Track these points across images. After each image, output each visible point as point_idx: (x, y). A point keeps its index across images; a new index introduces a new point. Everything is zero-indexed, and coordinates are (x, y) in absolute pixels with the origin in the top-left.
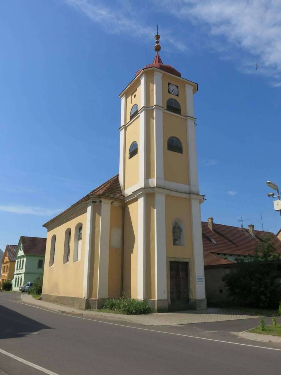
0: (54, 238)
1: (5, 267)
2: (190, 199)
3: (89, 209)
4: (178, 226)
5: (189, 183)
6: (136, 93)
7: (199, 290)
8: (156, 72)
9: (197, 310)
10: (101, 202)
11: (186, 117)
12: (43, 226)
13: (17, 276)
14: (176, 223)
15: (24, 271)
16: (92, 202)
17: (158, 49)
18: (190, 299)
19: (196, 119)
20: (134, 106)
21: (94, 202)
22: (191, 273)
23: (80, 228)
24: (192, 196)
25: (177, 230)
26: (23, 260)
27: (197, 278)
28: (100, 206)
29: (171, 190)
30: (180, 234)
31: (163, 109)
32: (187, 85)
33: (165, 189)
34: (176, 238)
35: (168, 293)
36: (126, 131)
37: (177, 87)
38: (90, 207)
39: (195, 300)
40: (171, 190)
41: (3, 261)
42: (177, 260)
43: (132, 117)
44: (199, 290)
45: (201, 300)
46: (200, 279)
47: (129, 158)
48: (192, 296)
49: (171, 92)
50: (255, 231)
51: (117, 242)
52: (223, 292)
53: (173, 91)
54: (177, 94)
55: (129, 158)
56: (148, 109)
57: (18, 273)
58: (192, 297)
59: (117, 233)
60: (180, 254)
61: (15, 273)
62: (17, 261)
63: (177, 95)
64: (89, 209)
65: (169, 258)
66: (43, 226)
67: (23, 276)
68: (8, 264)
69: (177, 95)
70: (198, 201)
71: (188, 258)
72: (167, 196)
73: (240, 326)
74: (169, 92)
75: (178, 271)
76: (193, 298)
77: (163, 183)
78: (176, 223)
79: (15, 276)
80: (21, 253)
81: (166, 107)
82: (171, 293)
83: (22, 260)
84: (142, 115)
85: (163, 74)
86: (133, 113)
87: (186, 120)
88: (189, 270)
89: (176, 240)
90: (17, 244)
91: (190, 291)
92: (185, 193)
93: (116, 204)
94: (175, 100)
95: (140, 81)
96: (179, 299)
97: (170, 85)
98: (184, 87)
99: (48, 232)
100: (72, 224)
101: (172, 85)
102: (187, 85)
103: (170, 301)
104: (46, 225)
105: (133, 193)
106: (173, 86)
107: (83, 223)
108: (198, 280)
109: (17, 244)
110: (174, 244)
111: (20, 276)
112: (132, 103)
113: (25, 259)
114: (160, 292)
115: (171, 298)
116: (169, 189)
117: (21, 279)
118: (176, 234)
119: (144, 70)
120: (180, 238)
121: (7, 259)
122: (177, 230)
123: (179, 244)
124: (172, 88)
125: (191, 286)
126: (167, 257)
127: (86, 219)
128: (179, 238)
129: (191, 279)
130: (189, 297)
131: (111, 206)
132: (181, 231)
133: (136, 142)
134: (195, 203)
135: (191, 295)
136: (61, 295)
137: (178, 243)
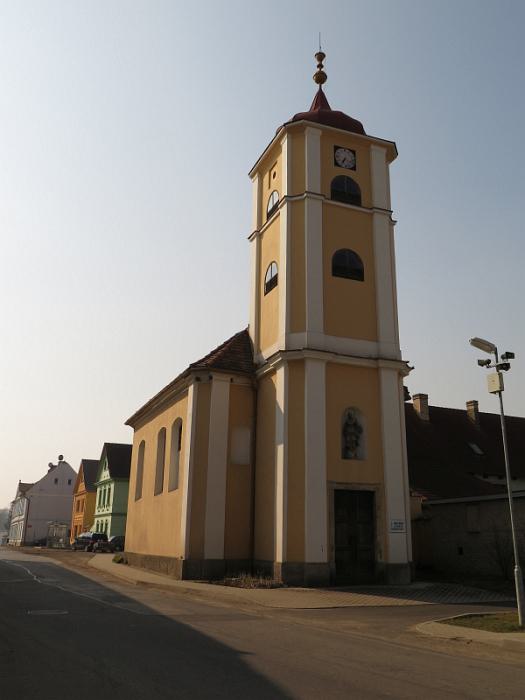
0: (143, 444)
1: (79, 501)
2: (377, 369)
3: (191, 389)
6: (275, 169)
7: (396, 545)
8: (308, 128)
10: (211, 378)
12: (127, 424)
13: (100, 519)
14: (350, 417)
15: (111, 511)
17: (321, 78)
21: (198, 379)
23: (178, 426)
24: (382, 364)
26: (109, 489)
28: (210, 385)
29: (336, 354)
30: (357, 437)
31: (323, 198)
32: (372, 147)
33: (328, 352)
36: (263, 241)
37: (354, 152)
38: (192, 387)
39: (388, 566)
40: (336, 354)
41: (76, 490)
42: (350, 488)
44: (396, 545)
45: (398, 567)
46: (398, 526)
47: (265, 294)
49: (340, 162)
55: (265, 294)
56: (293, 199)
57: (101, 513)
58: (380, 560)
59: (243, 438)
60: (355, 475)
61: (97, 513)
62: (98, 490)
63: (354, 168)
64: (191, 389)
66: (127, 424)
67: (109, 518)
68: (84, 497)
69: (354, 168)
70: (396, 373)
71: (372, 482)
72: (329, 364)
73: (422, 615)
74: (336, 164)
75: (354, 508)
76: (383, 560)
77: (321, 340)
78: (350, 417)
79: (96, 520)
80: (105, 475)
81: (328, 194)
82: (338, 550)
83: (107, 487)
84: (283, 211)
85: (323, 130)
87: (372, 214)
90: (99, 458)
92: (370, 358)
93: (240, 381)
94: (348, 178)
95: (281, 147)
96: (353, 565)
97: (339, 151)
100: (165, 419)
102: (372, 147)
103: (333, 566)
104: (129, 423)
109: (99, 458)
110: (345, 456)
111: (104, 519)
113: (112, 486)
114: (318, 549)
116: (331, 350)
117: (106, 525)
118: (351, 435)
120: (357, 444)
121: (82, 487)
122: (351, 430)
123: (356, 457)
124: (342, 155)
127: (186, 408)
135: (379, 556)
136: (152, 552)
137: (352, 454)
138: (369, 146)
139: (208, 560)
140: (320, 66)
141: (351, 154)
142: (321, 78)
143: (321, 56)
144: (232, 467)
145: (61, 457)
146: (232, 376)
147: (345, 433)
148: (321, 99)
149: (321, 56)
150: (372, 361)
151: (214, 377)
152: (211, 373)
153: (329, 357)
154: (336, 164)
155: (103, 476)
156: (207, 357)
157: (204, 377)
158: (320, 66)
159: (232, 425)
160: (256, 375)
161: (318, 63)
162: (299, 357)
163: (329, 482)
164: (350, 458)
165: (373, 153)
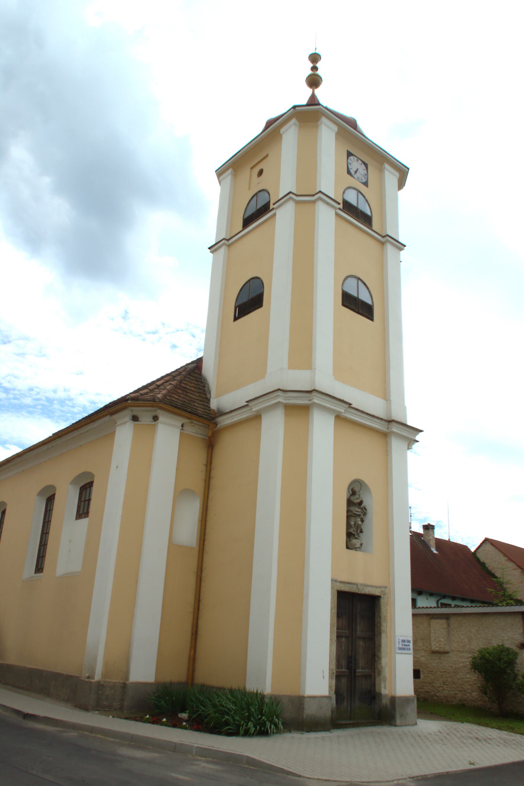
4: (358, 501)
5: (385, 395)
9: (395, 726)
10: (155, 418)
11: (383, 237)
14: (353, 493)
16: (131, 418)
18: (380, 694)
19: (405, 246)
20: (256, 194)
21: (135, 418)
22: (385, 626)
25: (356, 510)
27: (397, 640)
30: (362, 521)
32: (387, 166)
34: (351, 530)
35: (331, 677)
37: (366, 165)
39: (393, 699)
42: (354, 589)
43: (247, 222)
45: (406, 700)
48: (385, 688)
49: (352, 172)
50: (436, 539)
51: (188, 534)
52: (422, 676)
53: (358, 172)
54: (364, 181)
58: (385, 691)
59: (192, 511)
60: (363, 575)
63: (366, 184)
65: (336, 581)
69: (366, 184)
74: (349, 172)
86: (252, 210)
88: (380, 617)
89: (354, 535)
91: (379, 673)
98: (381, 171)
99: (199, 361)
101: (356, 159)
103: (334, 697)
105: (247, 402)
106: (357, 160)
107: (94, 473)
108: (401, 646)
112: (249, 189)
115: (338, 692)
119: (297, 108)
120: (361, 532)
125: (385, 661)
126: (332, 580)
128: (359, 532)
129: (385, 641)
130: (377, 690)
131: (181, 432)
132: (365, 514)
133: (408, 169)
134: (396, 444)
135: (383, 685)
138: (382, 164)
139: (132, 683)
140: (314, 68)
141: (363, 166)
142: (314, 81)
143: (315, 58)
144: (173, 548)
145: (417, 441)
146: (185, 421)
147: (350, 515)
148: (313, 101)
149: (315, 58)
150: (383, 422)
151: (161, 419)
152: (159, 412)
153: (341, 409)
154: (349, 172)
155: (184, 717)
156: (158, 380)
157: (146, 419)
158: (314, 68)
159: (181, 493)
160: (216, 424)
161: (311, 65)
162: (305, 402)
163: (334, 581)
164: (356, 549)
165: (386, 173)
